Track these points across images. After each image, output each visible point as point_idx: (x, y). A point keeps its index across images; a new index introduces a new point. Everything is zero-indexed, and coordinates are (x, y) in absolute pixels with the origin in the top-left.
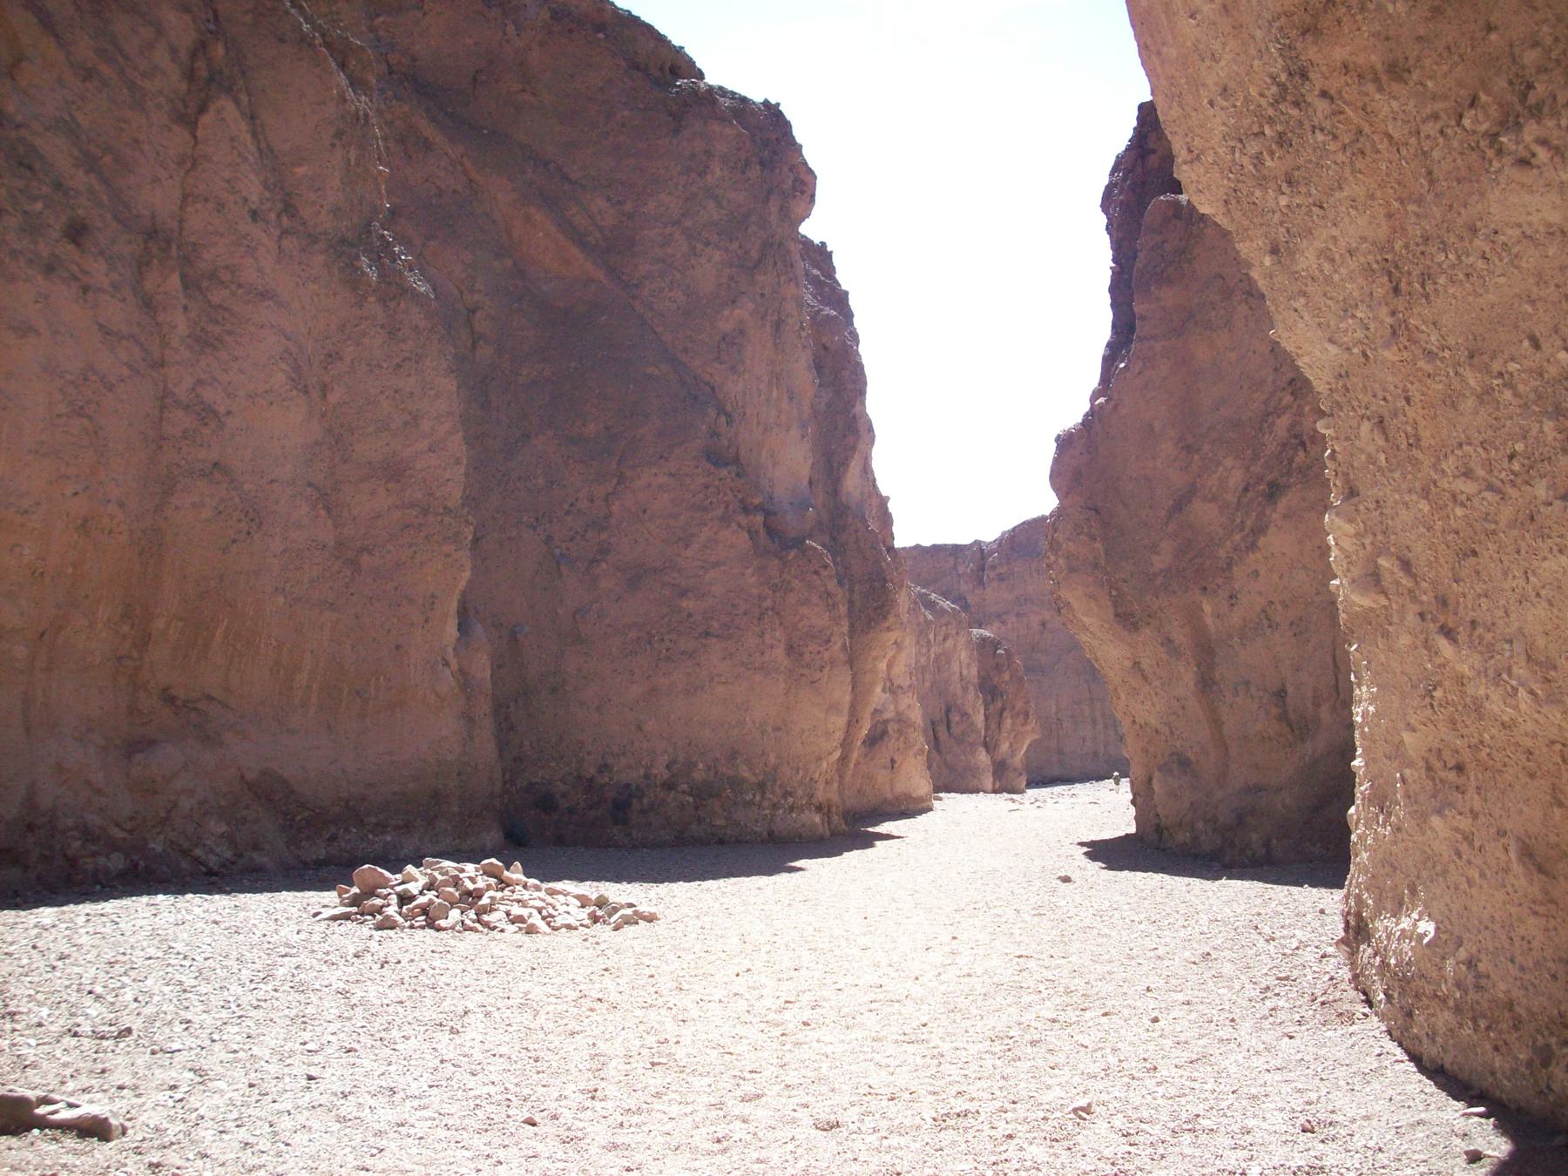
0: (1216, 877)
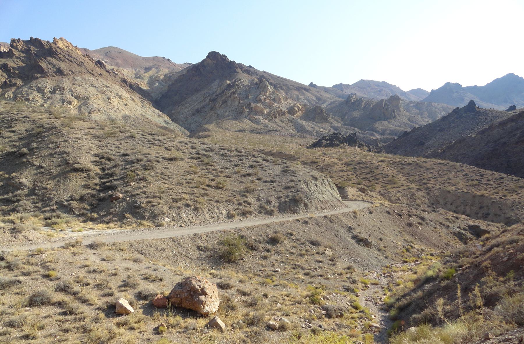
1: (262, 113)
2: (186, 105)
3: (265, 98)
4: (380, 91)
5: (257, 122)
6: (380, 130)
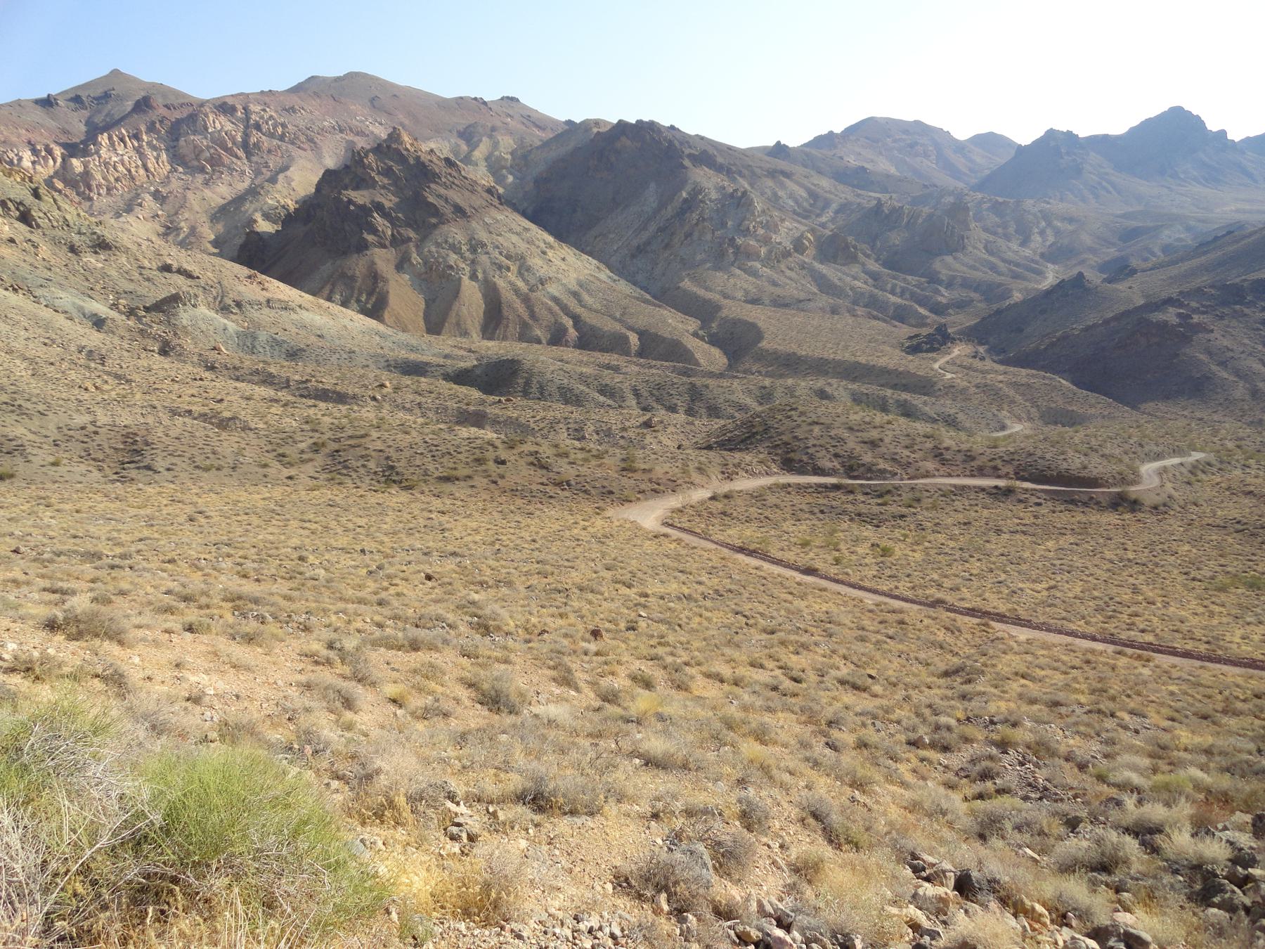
1: (758, 258)
2: (612, 236)
3: (754, 227)
4: (912, 145)
5: (753, 273)
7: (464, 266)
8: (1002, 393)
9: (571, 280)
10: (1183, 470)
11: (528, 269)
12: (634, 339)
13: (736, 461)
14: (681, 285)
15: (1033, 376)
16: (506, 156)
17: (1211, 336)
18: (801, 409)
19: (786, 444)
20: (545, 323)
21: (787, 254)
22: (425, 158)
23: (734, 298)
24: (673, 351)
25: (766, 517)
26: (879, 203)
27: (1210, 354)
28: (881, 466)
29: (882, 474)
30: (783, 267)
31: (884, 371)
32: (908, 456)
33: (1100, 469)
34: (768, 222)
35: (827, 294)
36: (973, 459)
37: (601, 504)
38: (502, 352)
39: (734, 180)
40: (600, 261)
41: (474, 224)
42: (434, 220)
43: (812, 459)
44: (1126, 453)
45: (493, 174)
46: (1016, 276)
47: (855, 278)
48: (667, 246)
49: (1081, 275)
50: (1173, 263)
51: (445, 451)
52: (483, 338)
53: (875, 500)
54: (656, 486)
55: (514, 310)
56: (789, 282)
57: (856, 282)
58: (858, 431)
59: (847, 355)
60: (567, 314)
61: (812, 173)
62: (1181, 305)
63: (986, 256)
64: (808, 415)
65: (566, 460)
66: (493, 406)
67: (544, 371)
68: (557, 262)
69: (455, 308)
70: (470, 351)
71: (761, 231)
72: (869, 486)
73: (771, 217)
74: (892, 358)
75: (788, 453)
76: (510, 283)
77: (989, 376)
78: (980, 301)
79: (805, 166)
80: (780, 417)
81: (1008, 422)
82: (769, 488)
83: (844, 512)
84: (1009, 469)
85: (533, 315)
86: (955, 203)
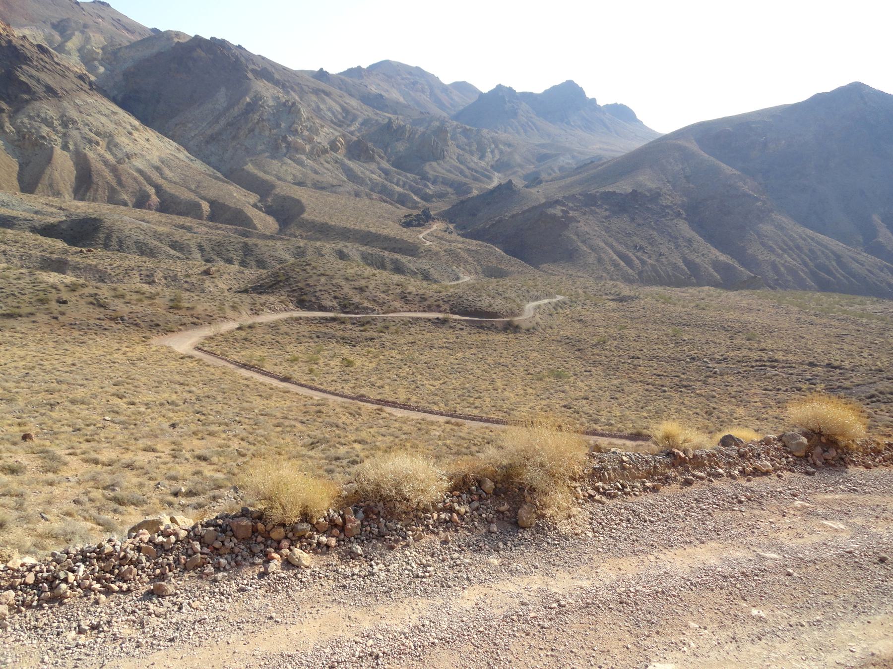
0: (851, 84)
1: (303, 152)
2: (190, 125)
3: (301, 129)
4: (414, 83)
5: (300, 163)
6: (431, 177)
7: (56, 137)
8: (460, 256)
9: (154, 157)
10: (550, 307)
11: (116, 145)
12: (205, 206)
13: (262, 301)
14: (245, 167)
15: (480, 245)
16: (97, 50)
17: (579, 224)
18: (313, 264)
19: (301, 289)
20: (130, 190)
21: (325, 151)
22: (16, 42)
23: (285, 181)
24: (238, 218)
25: (277, 342)
26: (390, 121)
27: (578, 236)
28: (365, 305)
29: (365, 310)
30: (322, 161)
31: (387, 238)
32: (384, 298)
33: (500, 307)
34: (311, 126)
35: (353, 182)
36: (425, 300)
37: (148, 334)
38: (90, 211)
39: (287, 93)
40: (179, 144)
41: (65, 104)
42: (26, 97)
43: (318, 300)
44: (518, 297)
45: (86, 64)
46: (476, 179)
47: (373, 173)
48: (234, 138)
49: (510, 181)
50: (562, 178)
51: (9, 293)
52: (75, 199)
53: (359, 328)
54: (196, 320)
55: (104, 177)
56: (326, 171)
57: (373, 175)
58: (352, 281)
59: (363, 226)
60: (150, 184)
61: (345, 94)
62: (564, 205)
63: (458, 164)
64: (318, 269)
65: (122, 300)
66: (75, 255)
67: (122, 228)
68: (142, 142)
69: (48, 171)
70: (61, 208)
71: (306, 133)
72: (356, 318)
73: (314, 123)
74: (393, 230)
75: (302, 295)
76: (99, 155)
77: (453, 244)
78: (453, 194)
79: (341, 89)
80: (298, 270)
81: (461, 275)
82: (286, 320)
83: (333, 337)
84: (447, 307)
85: (120, 183)
86: (438, 127)
